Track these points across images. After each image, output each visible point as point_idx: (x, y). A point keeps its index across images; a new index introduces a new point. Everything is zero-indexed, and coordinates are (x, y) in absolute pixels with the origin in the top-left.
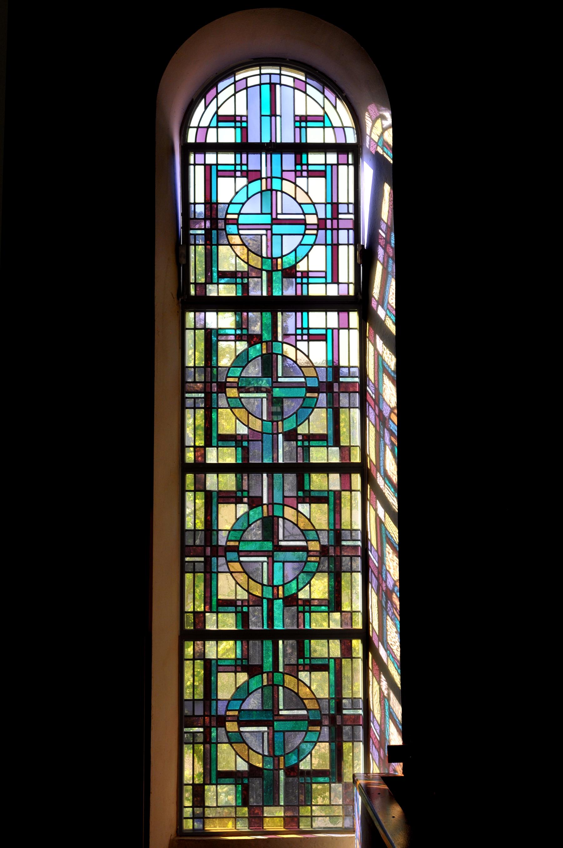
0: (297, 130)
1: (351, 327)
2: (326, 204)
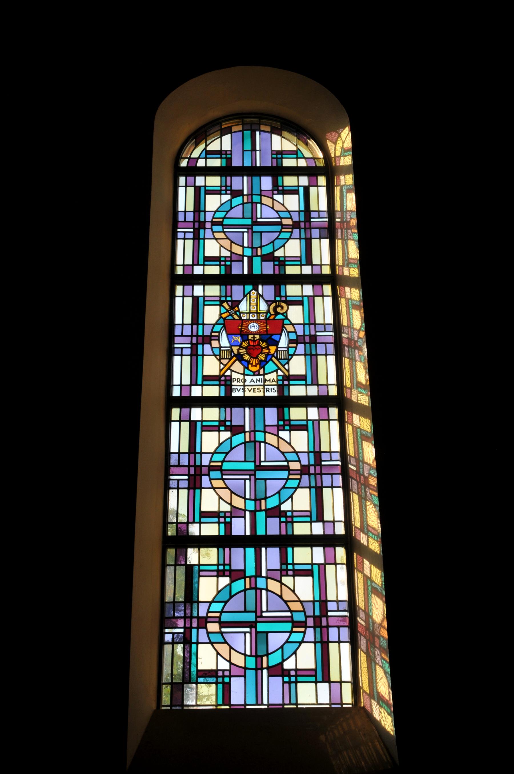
0: (286, 686)
1: (330, 418)
2: (308, 453)
